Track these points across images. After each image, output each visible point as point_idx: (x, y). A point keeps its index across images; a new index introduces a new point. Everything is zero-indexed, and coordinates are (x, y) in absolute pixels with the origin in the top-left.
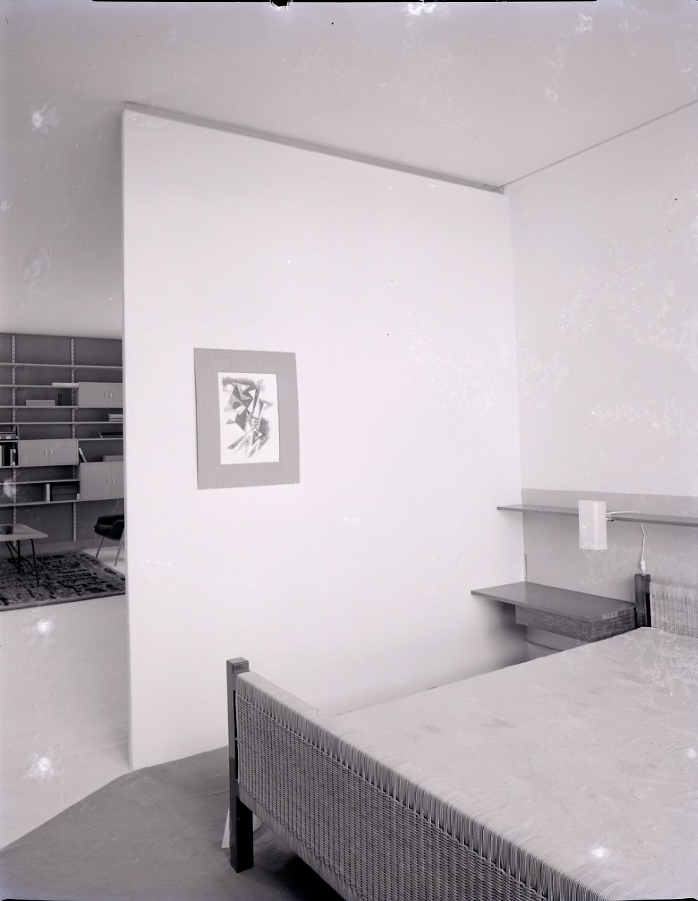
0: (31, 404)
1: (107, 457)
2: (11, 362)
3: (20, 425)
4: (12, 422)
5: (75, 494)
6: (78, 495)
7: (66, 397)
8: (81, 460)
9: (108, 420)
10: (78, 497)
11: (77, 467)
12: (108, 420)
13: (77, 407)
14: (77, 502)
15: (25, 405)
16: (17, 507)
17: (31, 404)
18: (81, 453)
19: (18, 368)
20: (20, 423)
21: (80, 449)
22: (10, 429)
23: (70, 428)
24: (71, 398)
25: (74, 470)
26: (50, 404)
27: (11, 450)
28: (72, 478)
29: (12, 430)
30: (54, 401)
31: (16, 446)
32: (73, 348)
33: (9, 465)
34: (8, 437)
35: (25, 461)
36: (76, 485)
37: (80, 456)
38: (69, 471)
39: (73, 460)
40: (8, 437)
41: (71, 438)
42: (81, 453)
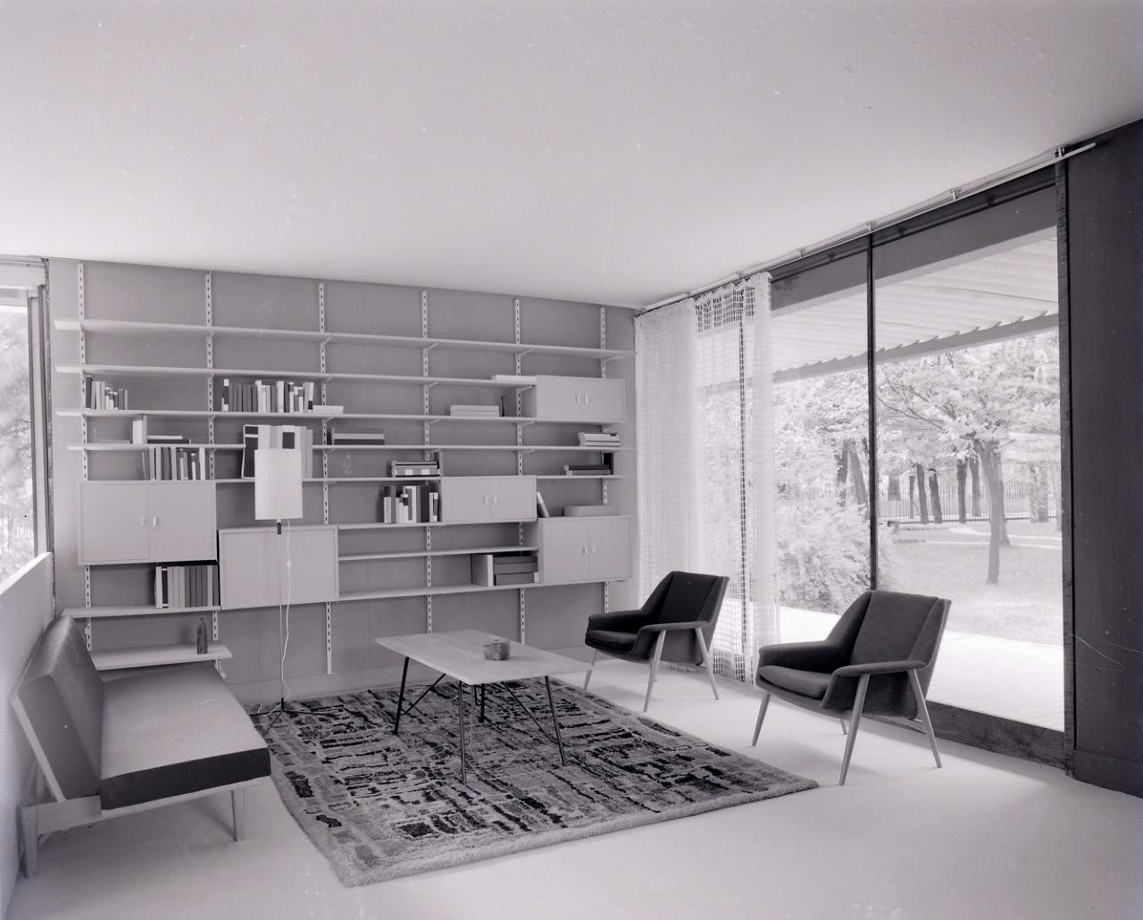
0: (460, 413)
1: (581, 509)
2: (319, 331)
3: (443, 450)
4: (423, 444)
5: (532, 573)
6: (536, 574)
7: (509, 401)
8: (540, 514)
9: (577, 443)
10: (536, 579)
11: (529, 527)
12: (577, 443)
13: (533, 419)
14: (222, 612)
15: (449, 414)
16: (94, 619)
17: (460, 413)
18: (541, 501)
19: (331, 344)
20: (443, 447)
21: (539, 494)
22: (419, 457)
23: (513, 456)
24: (515, 405)
25: (521, 530)
26: (491, 413)
27: (431, 494)
28: (517, 544)
29: (423, 460)
30: (497, 408)
31: (434, 487)
32: (517, 315)
33: (428, 521)
34: (425, 471)
35: (452, 515)
36: (531, 557)
37: (539, 507)
38: (511, 530)
39: (526, 514)
40: (425, 471)
41: (517, 474)
42: (541, 501)
